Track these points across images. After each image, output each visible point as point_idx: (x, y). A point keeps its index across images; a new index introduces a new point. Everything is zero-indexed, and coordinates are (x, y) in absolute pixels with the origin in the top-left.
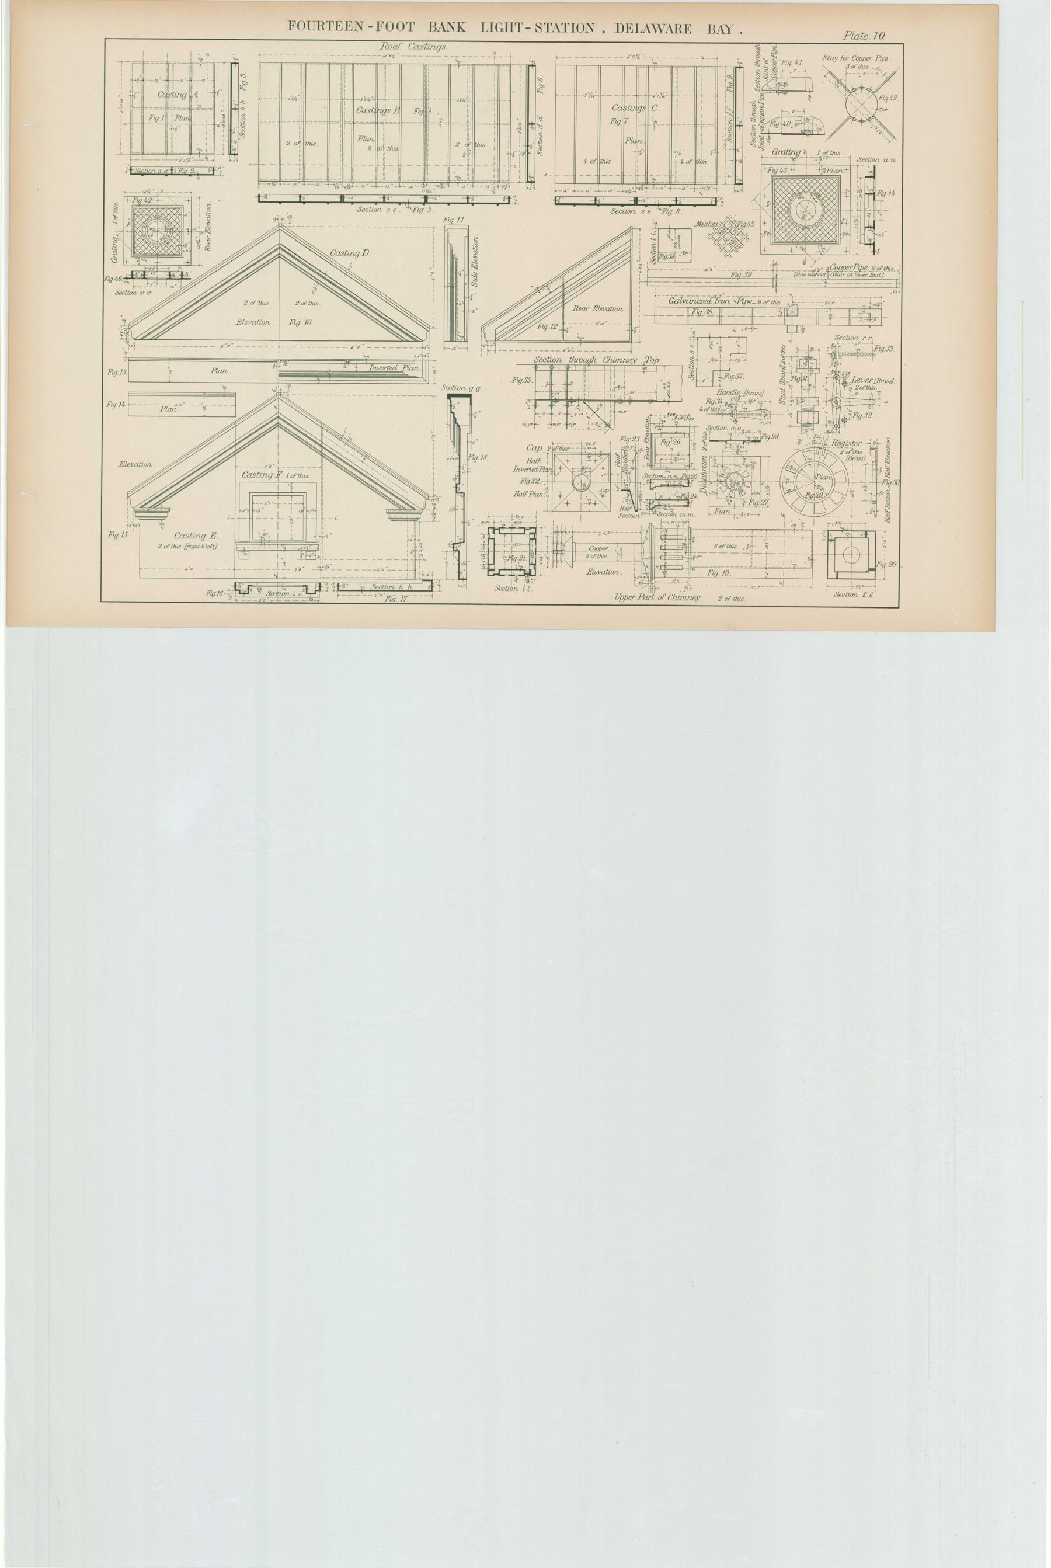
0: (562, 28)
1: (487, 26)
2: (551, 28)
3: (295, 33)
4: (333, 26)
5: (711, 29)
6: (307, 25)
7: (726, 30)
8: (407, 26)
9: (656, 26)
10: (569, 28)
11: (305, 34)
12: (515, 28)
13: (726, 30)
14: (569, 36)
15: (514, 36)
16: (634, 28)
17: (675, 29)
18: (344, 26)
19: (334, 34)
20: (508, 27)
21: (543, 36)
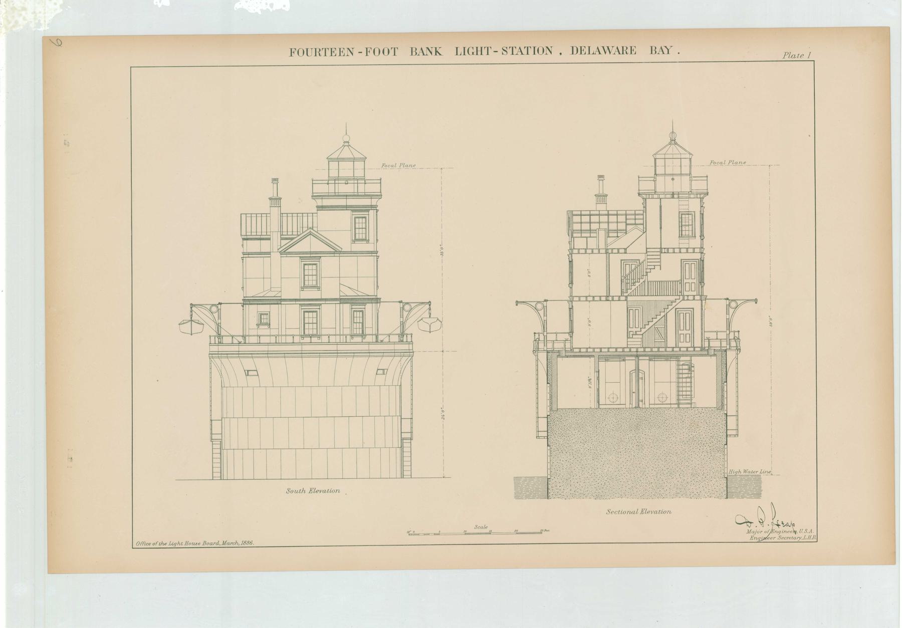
0: (525, 51)
1: (461, 50)
2: (515, 51)
3: (296, 59)
4: (328, 53)
5: (653, 50)
6: (306, 52)
7: (665, 51)
8: (392, 52)
9: (606, 49)
10: (531, 51)
11: (304, 60)
12: (484, 52)
13: (665, 51)
14: (531, 58)
15: (483, 58)
16: (587, 50)
17: (622, 51)
18: (337, 52)
19: (329, 60)
20: (479, 51)
21: (508, 58)
